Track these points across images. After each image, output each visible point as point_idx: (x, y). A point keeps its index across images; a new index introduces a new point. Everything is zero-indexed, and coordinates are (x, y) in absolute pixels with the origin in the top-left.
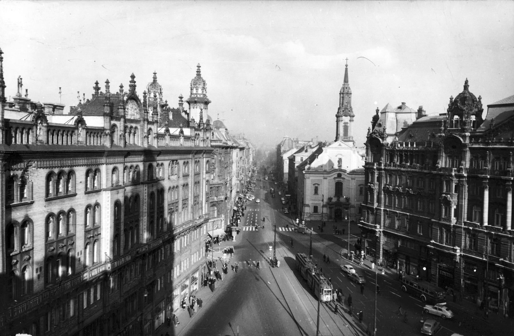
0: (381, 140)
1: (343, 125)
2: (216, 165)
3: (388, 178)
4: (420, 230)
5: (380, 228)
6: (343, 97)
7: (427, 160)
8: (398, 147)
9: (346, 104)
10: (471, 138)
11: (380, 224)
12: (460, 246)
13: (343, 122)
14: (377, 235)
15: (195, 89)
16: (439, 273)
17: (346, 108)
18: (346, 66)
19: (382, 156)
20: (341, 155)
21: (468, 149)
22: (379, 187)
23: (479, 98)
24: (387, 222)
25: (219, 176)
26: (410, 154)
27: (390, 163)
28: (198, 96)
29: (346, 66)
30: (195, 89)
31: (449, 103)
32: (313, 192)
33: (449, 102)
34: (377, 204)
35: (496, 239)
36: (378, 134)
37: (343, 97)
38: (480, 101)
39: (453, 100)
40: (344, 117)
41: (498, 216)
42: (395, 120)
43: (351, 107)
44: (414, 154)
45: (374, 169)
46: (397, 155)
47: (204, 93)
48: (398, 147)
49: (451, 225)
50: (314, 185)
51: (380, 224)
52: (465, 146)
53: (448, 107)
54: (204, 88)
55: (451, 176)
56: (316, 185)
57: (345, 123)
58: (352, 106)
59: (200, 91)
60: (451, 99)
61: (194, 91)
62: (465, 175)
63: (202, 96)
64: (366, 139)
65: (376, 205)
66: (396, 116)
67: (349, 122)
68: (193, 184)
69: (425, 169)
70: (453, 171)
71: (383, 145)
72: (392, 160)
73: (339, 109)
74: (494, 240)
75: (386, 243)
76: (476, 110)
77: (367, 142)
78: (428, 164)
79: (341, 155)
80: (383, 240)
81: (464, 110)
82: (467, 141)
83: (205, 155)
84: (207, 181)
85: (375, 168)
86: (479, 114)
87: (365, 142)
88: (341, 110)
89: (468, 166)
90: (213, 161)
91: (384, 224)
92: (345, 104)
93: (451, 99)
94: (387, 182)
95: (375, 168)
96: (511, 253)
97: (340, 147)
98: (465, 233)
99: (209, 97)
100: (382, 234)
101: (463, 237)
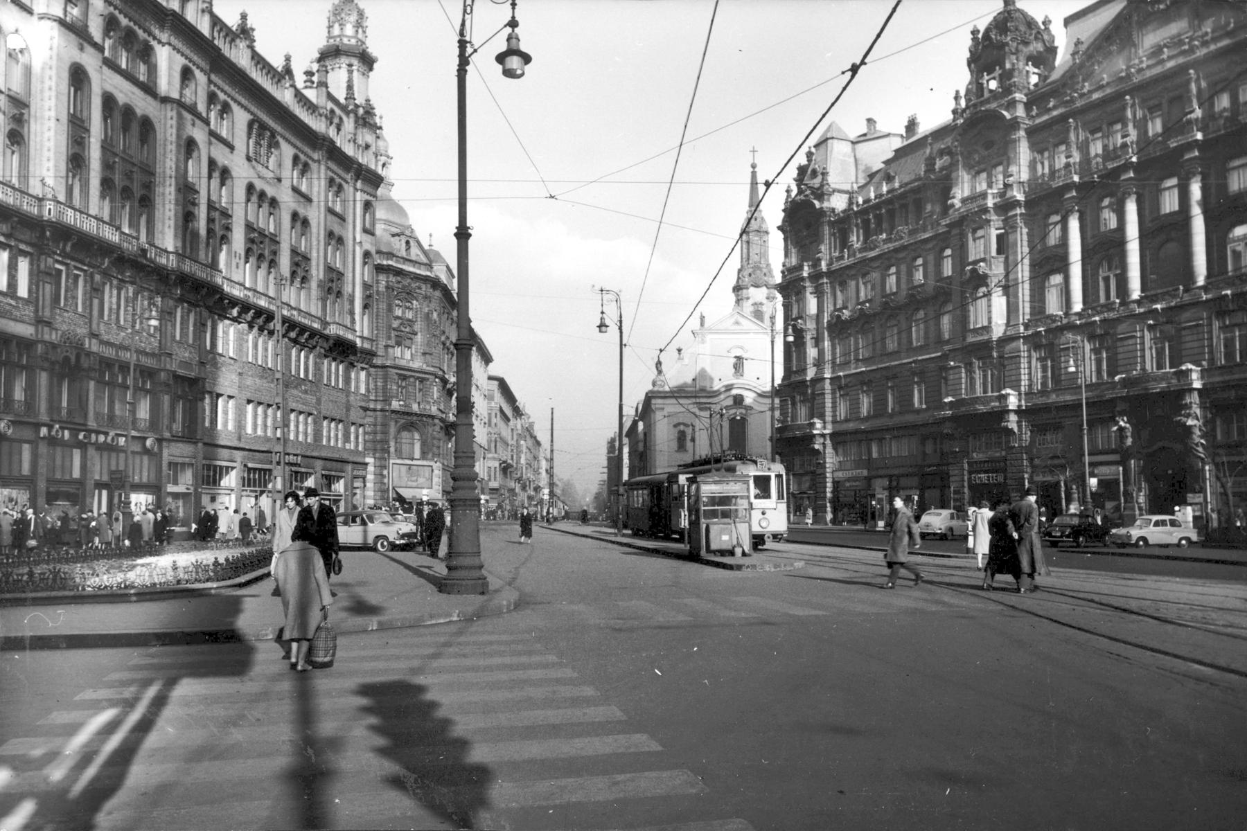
0: (816, 202)
1: (752, 309)
2: (417, 327)
3: (839, 293)
4: (920, 398)
5: (824, 428)
6: (748, 242)
7: (929, 207)
8: (858, 205)
9: (756, 258)
10: (1028, 106)
11: (822, 416)
12: (1016, 386)
13: (751, 302)
14: (817, 447)
15: (336, 26)
16: (970, 479)
17: (757, 268)
18: (754, 166)
19: (818, 239)
20: (741, 348)
21: (1022, 133)
22: (817, 323)
23: (1044, 23)
24: (842, 412)
25: (424, 354)
26: (888, 211)
27: (842, 251)
28: (345, 41)
29: (754, 166)
30: (336, 26)
31: (969, 43)
32: (674, 445)
33: (968, 42)
34: (814, 369)
35: (1107, 334)
36: (808, 192)
37: (748, 242)
38: (1047, 29)
39: (980, 36)
40: (752, 289)
41: (1107, 280)
42: (852, 160)
43: (768, 265)
44: (897, 205)
45: (803, 279)
46: (857, 225)
47: (360, 35)
48: (858, 205)
49: (989, 341)
50: (675, 426)
51: (822, 416)
52: (1014, 124)
53: (968, 55)
54: (359, 25)
55: (985, 210)
56: (682, 428)
57: (755, 304)
58: (771, 261)
59: (349, 30)
60: (973, 33)
61: (336, 30)
62: (1020, 197)
63: (353, 41)
64: (783, 214)
65: (811, 373)
66: (854, 150)
67: (765, 301)
68: (322, 236)
69: (925, 231)
70: (990, 197)
71: (822, 212)
72: (844, 244)
73: (740, 271)
74: (1101, 337)
75: (841, 467)
76: (1040, 47)
77: (784, 221)
78: (931, 216)
79: (741, 348)
80: (831, 459)
81: (1007, 44)
82: (1020, 111)
83: (359, 184)
84: (367, 254)
85: (805, 274)
86: (1044, 58)
87: (780, 223)
88: (746, 273)
89: (1025, 176)
90: (409, 315)
91: (834, 416)
92: (754, 258)
93: (975, 32)
94: (835, 304)
95: (805, 274)
96: (1143, 357)
97: (737, 327)
98: (1029, 351)
99: (373, 50)
100: (828, 442)
101: (1024, 363)
